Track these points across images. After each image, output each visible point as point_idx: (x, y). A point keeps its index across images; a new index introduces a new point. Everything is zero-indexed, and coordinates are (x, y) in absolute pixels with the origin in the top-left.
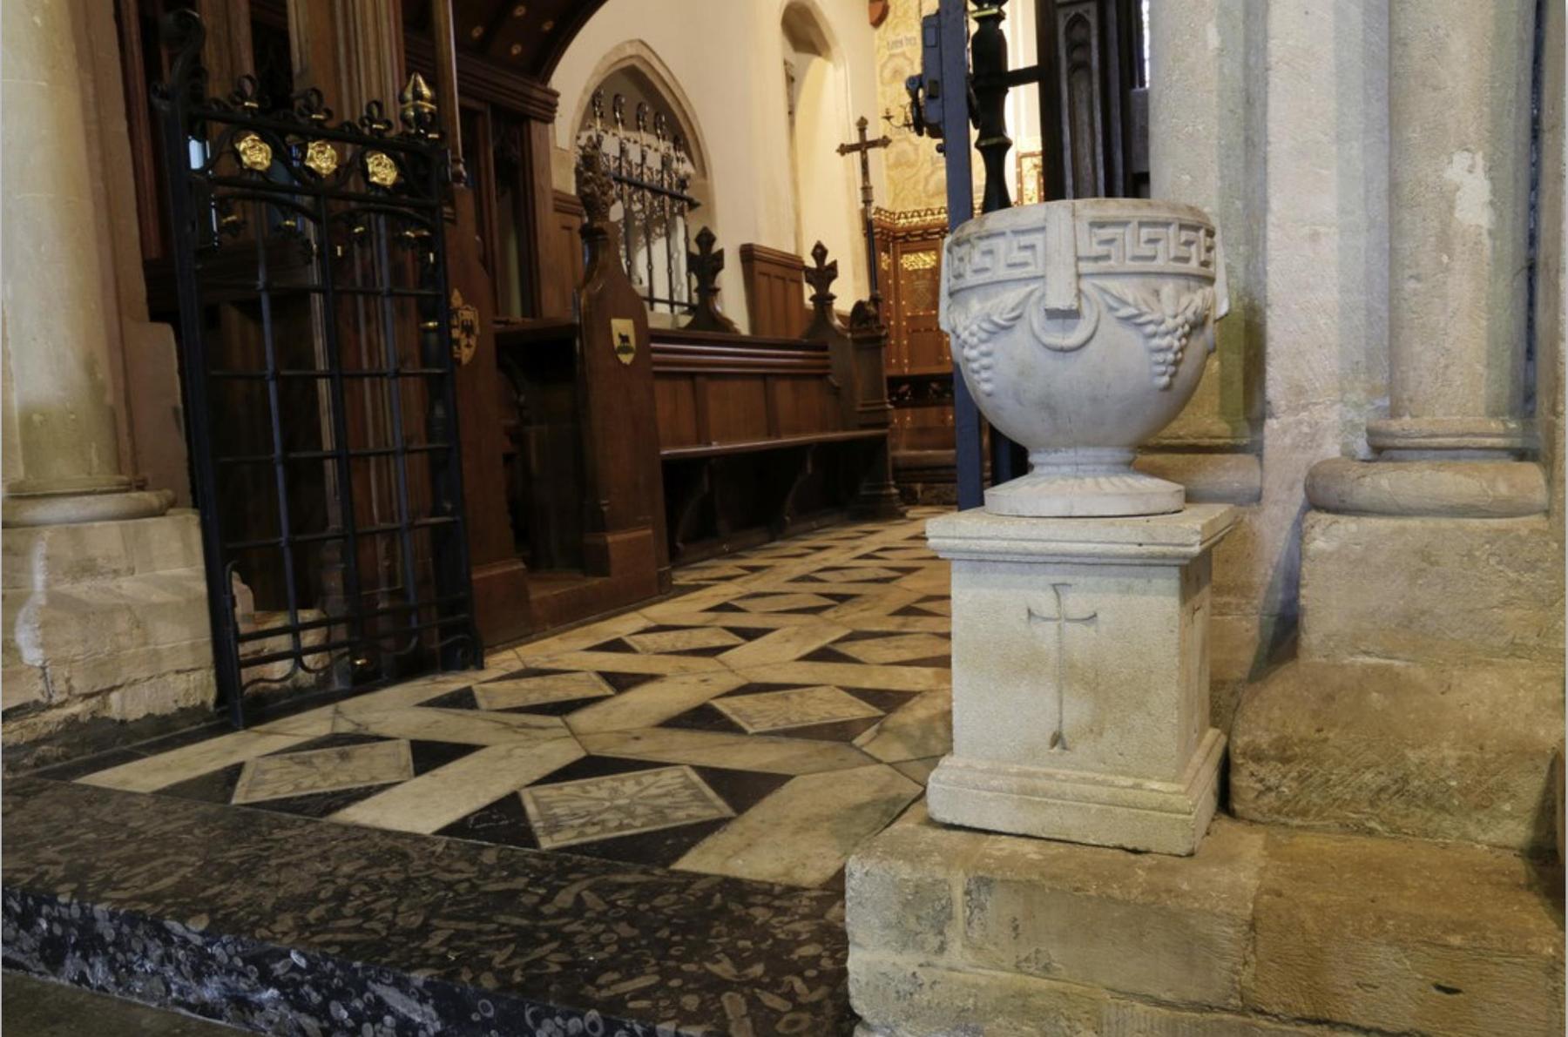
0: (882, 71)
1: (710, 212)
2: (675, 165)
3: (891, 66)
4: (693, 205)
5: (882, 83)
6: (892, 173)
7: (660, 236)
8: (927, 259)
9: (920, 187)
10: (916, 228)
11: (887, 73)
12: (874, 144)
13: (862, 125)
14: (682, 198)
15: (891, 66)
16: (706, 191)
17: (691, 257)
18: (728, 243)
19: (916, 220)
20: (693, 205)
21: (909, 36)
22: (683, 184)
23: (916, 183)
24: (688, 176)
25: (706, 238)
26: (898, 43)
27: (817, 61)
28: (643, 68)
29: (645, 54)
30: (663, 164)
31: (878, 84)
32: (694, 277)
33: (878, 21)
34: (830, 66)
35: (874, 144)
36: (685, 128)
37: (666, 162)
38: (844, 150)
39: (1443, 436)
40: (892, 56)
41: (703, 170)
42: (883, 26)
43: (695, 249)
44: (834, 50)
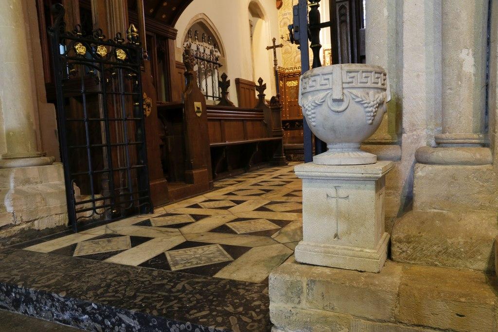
0: (280, 23)
1: (225, 68)
2: (214, 53)
3: (283, 22)
4: (220, 66)
5: (281, 27)
6: (283, 56)
7: (210, 76)
8: (295, 83)
9: (293, 60)
10: (291, 73)
11: (282, 24)
12: (278, 46)
13: (274, 40)
14: (217, 64)
15: (283, 22)
16: (224, 61)
17: (219, 82)
18: (231, 78)
19: (291, 70)
20: (220, 66)
21: (289, 12)
22: (217, 59)
23: (291, 59)
24: (219, 57)
25: (224, 76)
26: (285, 14)
27: (260, 20)
28: (204, 22)
29: (205, 18)
30: (211, 53)
31: (279, 27)
32: (220, 89)
33: (279, 8)
34: (264, 21)
35: (278, 46)
36: (218, 41)
37: (211, 52)
38: (268, 48)
39: (459, 139)
40: (283, 18)
41: (223, 55)
42: (281, 9)
43: (221, 80)
44: (265, 17)
